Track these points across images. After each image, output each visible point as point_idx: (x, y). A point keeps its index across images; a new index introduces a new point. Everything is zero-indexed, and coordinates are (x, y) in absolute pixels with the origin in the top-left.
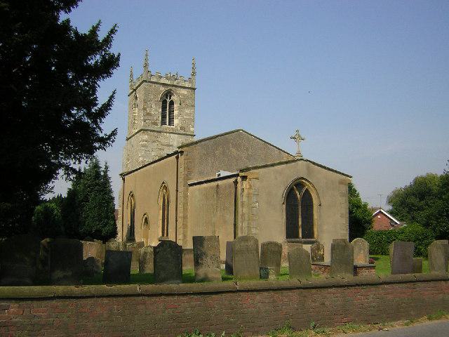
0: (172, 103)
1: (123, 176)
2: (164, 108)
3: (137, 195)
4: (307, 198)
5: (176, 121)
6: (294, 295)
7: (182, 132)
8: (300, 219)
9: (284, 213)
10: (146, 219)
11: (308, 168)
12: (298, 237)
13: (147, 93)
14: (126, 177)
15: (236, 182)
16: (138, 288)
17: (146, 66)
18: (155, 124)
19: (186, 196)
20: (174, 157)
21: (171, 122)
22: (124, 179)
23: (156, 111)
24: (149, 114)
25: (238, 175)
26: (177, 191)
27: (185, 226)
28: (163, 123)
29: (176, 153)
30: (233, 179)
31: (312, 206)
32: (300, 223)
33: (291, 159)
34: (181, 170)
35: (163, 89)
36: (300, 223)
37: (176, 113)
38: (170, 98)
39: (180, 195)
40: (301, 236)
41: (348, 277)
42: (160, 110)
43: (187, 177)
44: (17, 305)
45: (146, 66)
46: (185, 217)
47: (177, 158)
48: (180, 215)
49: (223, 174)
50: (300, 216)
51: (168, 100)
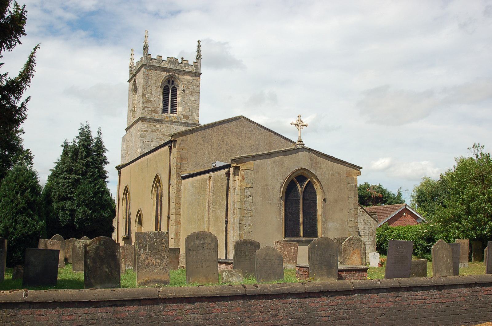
0: (175, 90)
1: (119, 168)
2: (166, 94)
3: (131, 190)
4: (310, 191)
5: (179, 109)
6: (238, 305)
7: (184, 121)
8: (301, 215)
9: (283, 209)
10: (140, 215)
11: (311, 159)
12: (298, 235)
13: (147, 77)
14: (122, 170)
15: (228, 174)
16: (71, 294)
17: (146, 48)
18: (156, 111)
19: (179, 191)
20: (167, 148)
21: (173, 111)
22: (120, 173)
23: (157, 97)
24: (148, 101)
25: (228, 166)
26: (169, 184)
27: (178, 223)
28: (165, 111)
29: (170, 142)
30: (226, 170)
31: (315, 200)
32: (301, 220)
33: (292, 146)
34: (174, 160)
35: (164, 74)
36: (301, 220)
37: (179, 99)
38: (173, 84)
39: (173, 188)
40: (301, 234)
41: (332, 282)
42: (161, 97)
43: (180, 169)
44: (357, 274)
45: (146, 48)
46: (178, 214)
47: (170, 148)
48: (173, 211)
49: (219, 164)
50: (301, 212)
51: (171, 87)
